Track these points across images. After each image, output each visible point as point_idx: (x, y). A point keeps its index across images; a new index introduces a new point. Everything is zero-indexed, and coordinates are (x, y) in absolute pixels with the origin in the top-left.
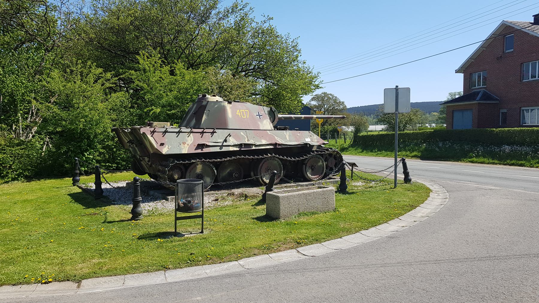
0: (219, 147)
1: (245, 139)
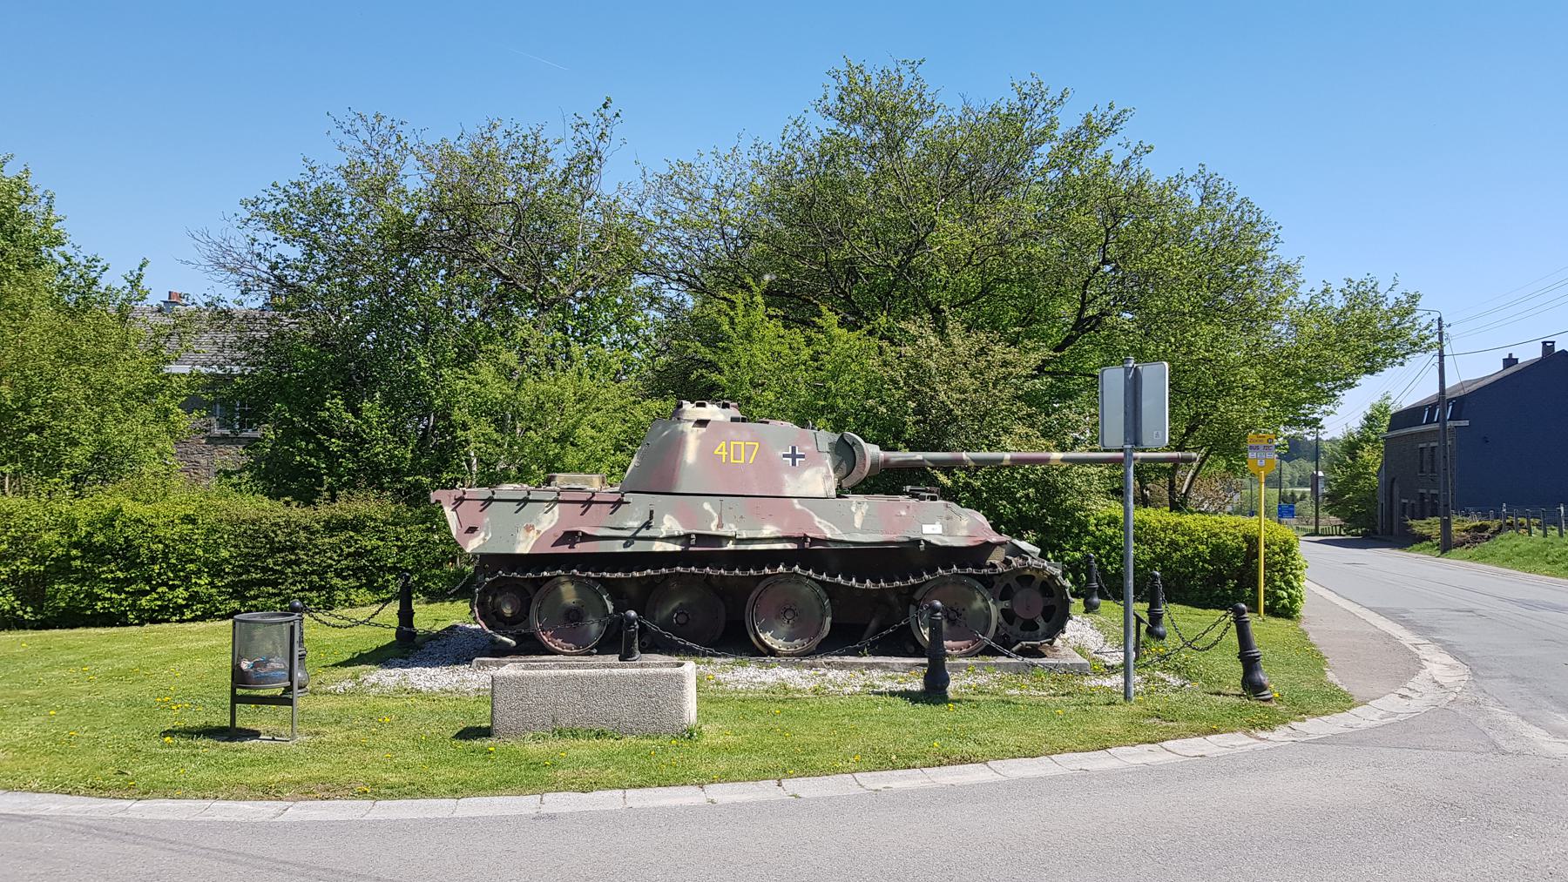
0: (624, 542)
1: (713, 520)
